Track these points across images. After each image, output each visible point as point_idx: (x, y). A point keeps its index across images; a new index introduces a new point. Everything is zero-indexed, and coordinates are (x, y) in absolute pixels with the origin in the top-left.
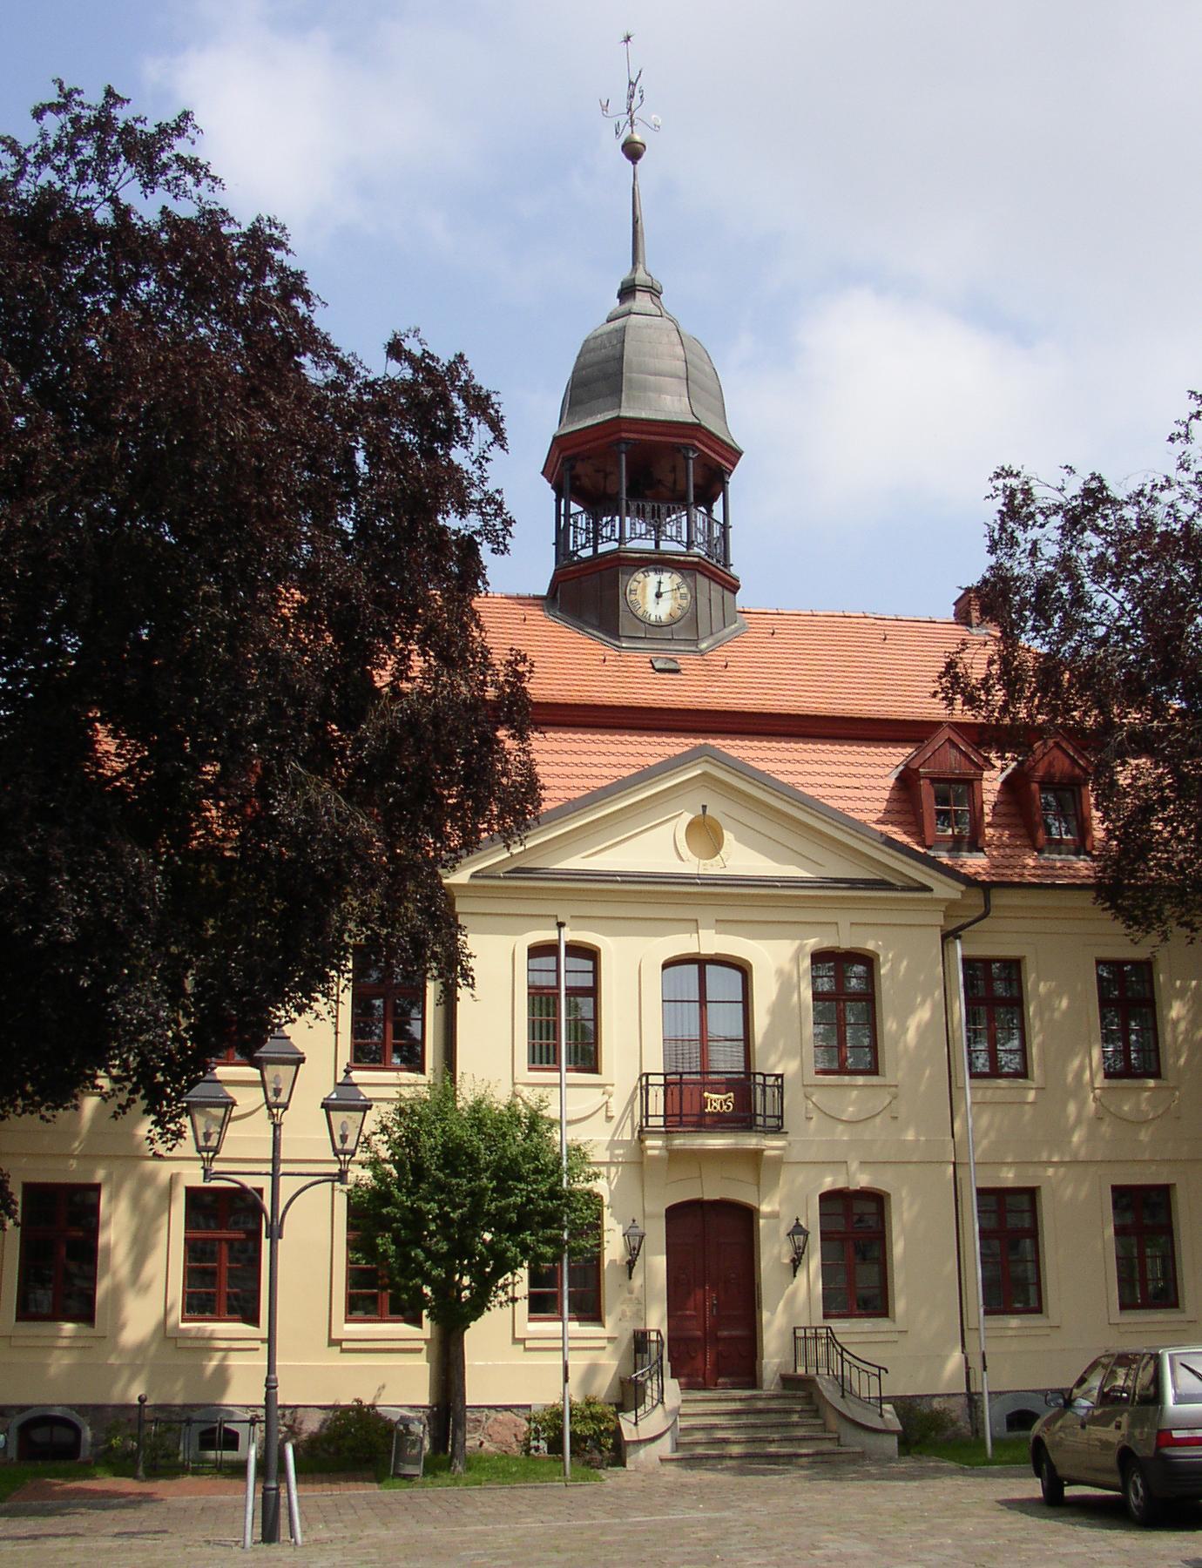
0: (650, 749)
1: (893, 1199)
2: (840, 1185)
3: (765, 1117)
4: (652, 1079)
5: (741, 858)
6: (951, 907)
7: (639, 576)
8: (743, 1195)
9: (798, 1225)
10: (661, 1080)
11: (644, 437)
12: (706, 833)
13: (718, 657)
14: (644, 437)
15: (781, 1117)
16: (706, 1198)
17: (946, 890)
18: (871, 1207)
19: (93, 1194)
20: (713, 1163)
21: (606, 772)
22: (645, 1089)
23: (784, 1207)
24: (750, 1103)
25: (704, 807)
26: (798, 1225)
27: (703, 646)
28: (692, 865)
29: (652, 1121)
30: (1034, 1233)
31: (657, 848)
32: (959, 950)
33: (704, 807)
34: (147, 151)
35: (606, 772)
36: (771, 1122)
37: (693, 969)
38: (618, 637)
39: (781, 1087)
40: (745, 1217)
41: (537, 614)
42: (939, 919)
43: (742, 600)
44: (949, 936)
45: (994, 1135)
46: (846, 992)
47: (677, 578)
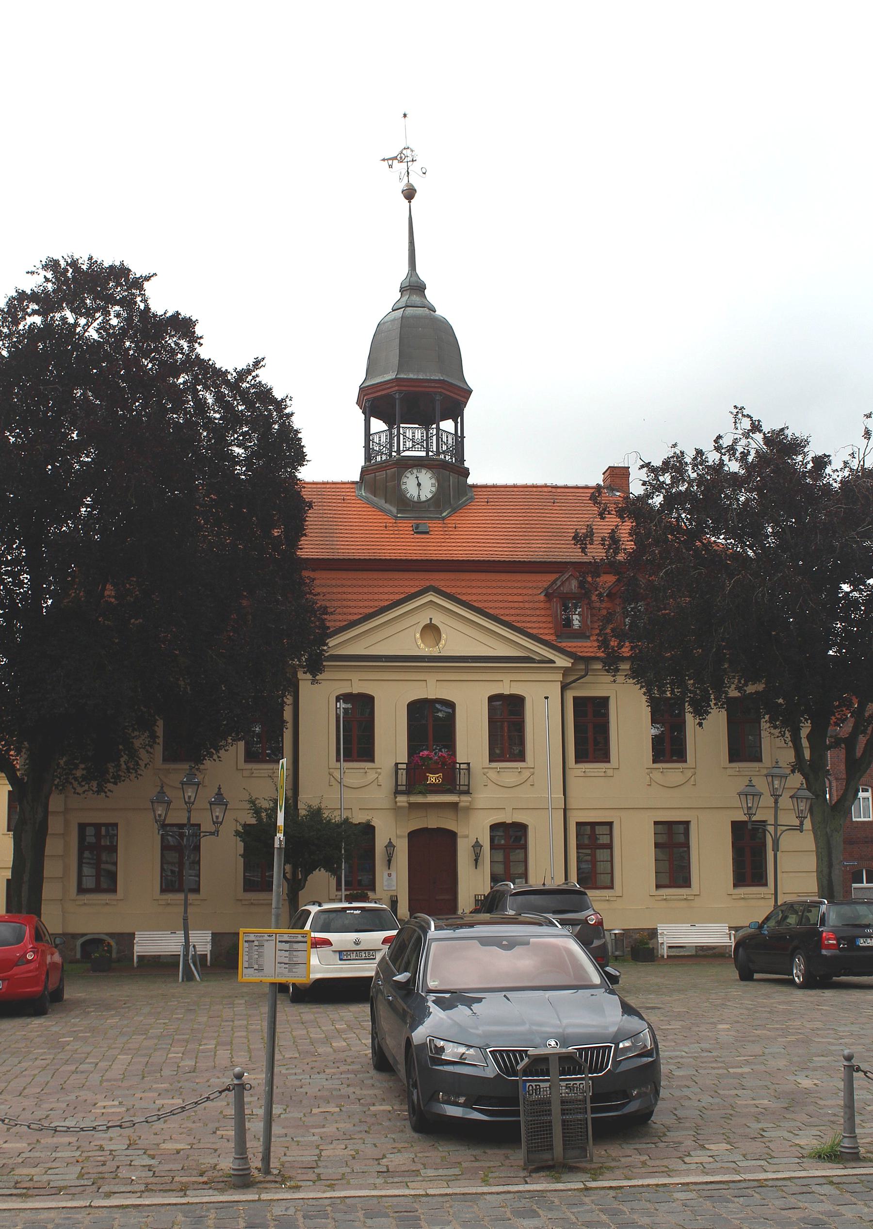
2: (425, 826)
3: (460, 785)
4: (400, 766)
6: (566, 671)
8: (451, 826)
10: (404, 766)
11: (412, 389)
13: (451, 522)
14: (412, 389)
15: (469, 785)
17: (562, 662)
18: (605, 829)
22: (397, 770)
23: (474, 831)
25: (431, 619)
27: (444, 514)
28: (425, 650)
29: (400, 788)
30: (687, 845)
32: (570, 695)
36: (466, 788)
39: (468, 769)
40: (450, 837)
41: (384, 299)
42: (560, 677)
43: (470, 481)
44: (564, 688)
45: (597, 792)
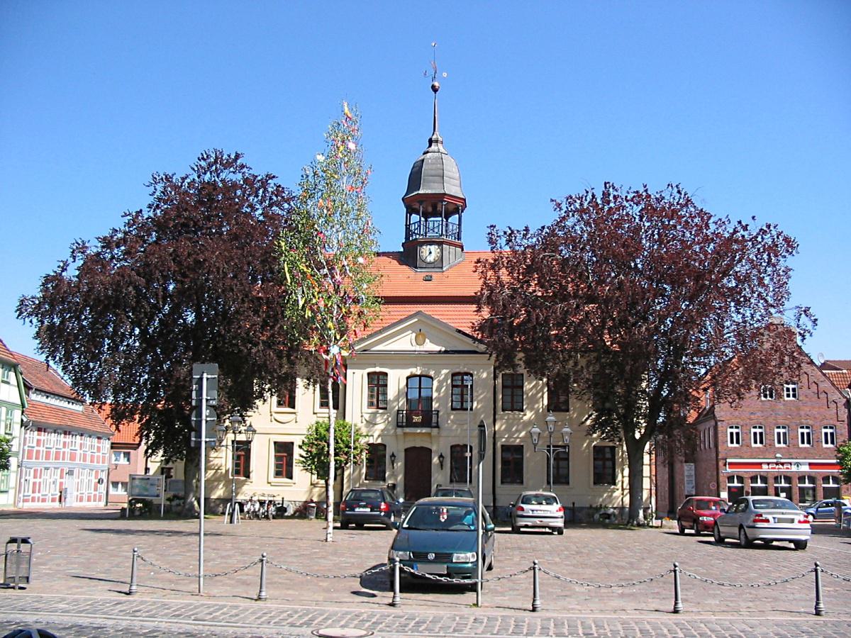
0: (411, 309)
1: (452, 444)
5: (429, 346)
7: (424, 247)
8: (429, 447)
9: (393, 454)
12: (419, 342)
16: (417, 446)
19: (733, 490)
20: (418, 437)
21: (404, 313)
24: (429, 419)
26: (393, 454)
31: (405, 342)
33: (420, 330)
34: (232, 162)
35: (404, 313)
37: (418, 378)
38: (416, 268)
46: (460, 383)
47: (437, 247)
